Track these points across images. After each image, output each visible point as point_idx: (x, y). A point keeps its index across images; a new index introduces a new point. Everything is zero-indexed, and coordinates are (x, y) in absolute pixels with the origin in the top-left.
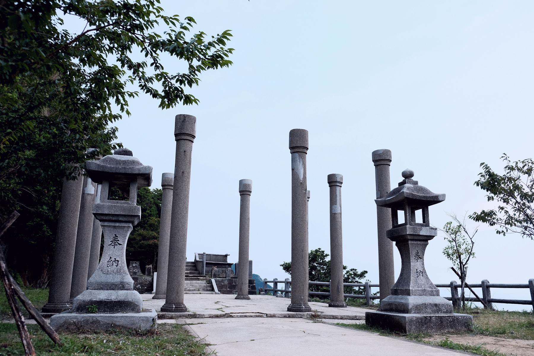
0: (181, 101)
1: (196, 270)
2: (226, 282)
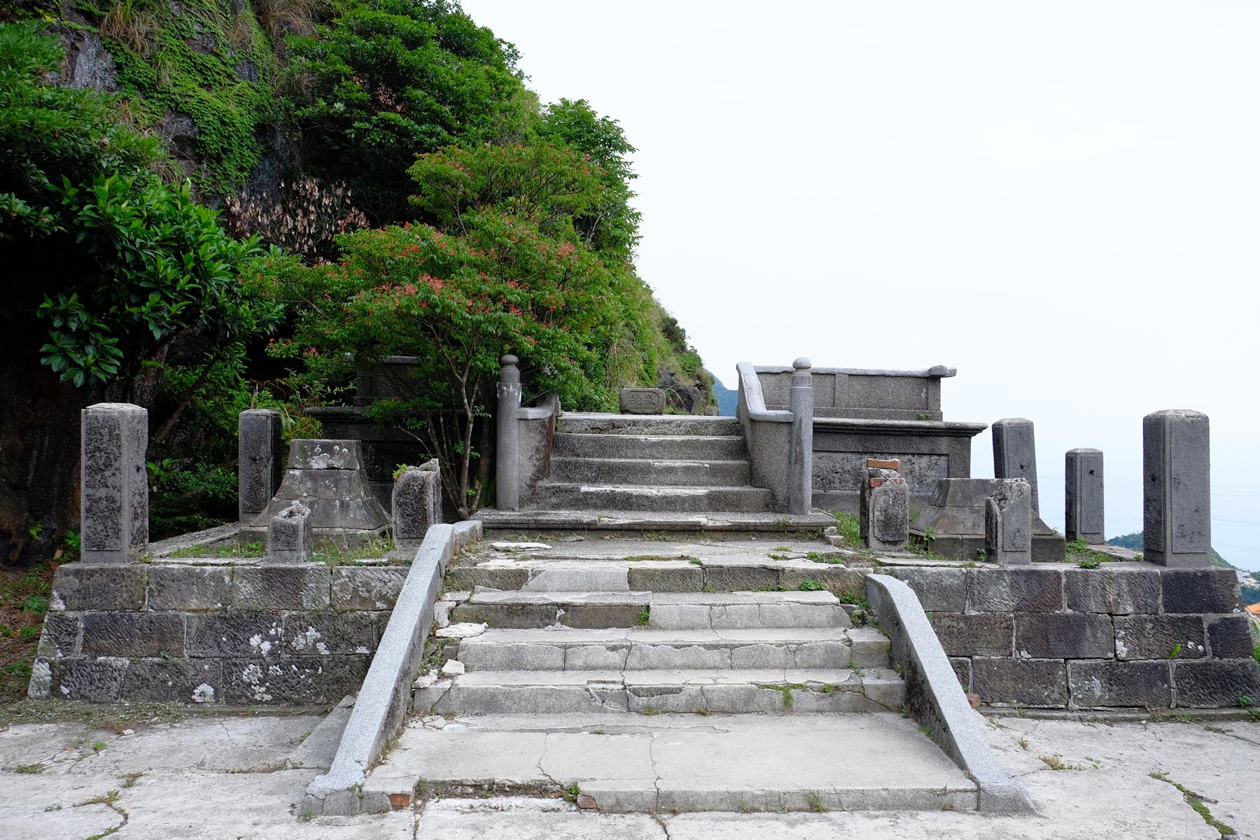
0: (390, 512)
1: (751, 476)
2: (1002, 600)
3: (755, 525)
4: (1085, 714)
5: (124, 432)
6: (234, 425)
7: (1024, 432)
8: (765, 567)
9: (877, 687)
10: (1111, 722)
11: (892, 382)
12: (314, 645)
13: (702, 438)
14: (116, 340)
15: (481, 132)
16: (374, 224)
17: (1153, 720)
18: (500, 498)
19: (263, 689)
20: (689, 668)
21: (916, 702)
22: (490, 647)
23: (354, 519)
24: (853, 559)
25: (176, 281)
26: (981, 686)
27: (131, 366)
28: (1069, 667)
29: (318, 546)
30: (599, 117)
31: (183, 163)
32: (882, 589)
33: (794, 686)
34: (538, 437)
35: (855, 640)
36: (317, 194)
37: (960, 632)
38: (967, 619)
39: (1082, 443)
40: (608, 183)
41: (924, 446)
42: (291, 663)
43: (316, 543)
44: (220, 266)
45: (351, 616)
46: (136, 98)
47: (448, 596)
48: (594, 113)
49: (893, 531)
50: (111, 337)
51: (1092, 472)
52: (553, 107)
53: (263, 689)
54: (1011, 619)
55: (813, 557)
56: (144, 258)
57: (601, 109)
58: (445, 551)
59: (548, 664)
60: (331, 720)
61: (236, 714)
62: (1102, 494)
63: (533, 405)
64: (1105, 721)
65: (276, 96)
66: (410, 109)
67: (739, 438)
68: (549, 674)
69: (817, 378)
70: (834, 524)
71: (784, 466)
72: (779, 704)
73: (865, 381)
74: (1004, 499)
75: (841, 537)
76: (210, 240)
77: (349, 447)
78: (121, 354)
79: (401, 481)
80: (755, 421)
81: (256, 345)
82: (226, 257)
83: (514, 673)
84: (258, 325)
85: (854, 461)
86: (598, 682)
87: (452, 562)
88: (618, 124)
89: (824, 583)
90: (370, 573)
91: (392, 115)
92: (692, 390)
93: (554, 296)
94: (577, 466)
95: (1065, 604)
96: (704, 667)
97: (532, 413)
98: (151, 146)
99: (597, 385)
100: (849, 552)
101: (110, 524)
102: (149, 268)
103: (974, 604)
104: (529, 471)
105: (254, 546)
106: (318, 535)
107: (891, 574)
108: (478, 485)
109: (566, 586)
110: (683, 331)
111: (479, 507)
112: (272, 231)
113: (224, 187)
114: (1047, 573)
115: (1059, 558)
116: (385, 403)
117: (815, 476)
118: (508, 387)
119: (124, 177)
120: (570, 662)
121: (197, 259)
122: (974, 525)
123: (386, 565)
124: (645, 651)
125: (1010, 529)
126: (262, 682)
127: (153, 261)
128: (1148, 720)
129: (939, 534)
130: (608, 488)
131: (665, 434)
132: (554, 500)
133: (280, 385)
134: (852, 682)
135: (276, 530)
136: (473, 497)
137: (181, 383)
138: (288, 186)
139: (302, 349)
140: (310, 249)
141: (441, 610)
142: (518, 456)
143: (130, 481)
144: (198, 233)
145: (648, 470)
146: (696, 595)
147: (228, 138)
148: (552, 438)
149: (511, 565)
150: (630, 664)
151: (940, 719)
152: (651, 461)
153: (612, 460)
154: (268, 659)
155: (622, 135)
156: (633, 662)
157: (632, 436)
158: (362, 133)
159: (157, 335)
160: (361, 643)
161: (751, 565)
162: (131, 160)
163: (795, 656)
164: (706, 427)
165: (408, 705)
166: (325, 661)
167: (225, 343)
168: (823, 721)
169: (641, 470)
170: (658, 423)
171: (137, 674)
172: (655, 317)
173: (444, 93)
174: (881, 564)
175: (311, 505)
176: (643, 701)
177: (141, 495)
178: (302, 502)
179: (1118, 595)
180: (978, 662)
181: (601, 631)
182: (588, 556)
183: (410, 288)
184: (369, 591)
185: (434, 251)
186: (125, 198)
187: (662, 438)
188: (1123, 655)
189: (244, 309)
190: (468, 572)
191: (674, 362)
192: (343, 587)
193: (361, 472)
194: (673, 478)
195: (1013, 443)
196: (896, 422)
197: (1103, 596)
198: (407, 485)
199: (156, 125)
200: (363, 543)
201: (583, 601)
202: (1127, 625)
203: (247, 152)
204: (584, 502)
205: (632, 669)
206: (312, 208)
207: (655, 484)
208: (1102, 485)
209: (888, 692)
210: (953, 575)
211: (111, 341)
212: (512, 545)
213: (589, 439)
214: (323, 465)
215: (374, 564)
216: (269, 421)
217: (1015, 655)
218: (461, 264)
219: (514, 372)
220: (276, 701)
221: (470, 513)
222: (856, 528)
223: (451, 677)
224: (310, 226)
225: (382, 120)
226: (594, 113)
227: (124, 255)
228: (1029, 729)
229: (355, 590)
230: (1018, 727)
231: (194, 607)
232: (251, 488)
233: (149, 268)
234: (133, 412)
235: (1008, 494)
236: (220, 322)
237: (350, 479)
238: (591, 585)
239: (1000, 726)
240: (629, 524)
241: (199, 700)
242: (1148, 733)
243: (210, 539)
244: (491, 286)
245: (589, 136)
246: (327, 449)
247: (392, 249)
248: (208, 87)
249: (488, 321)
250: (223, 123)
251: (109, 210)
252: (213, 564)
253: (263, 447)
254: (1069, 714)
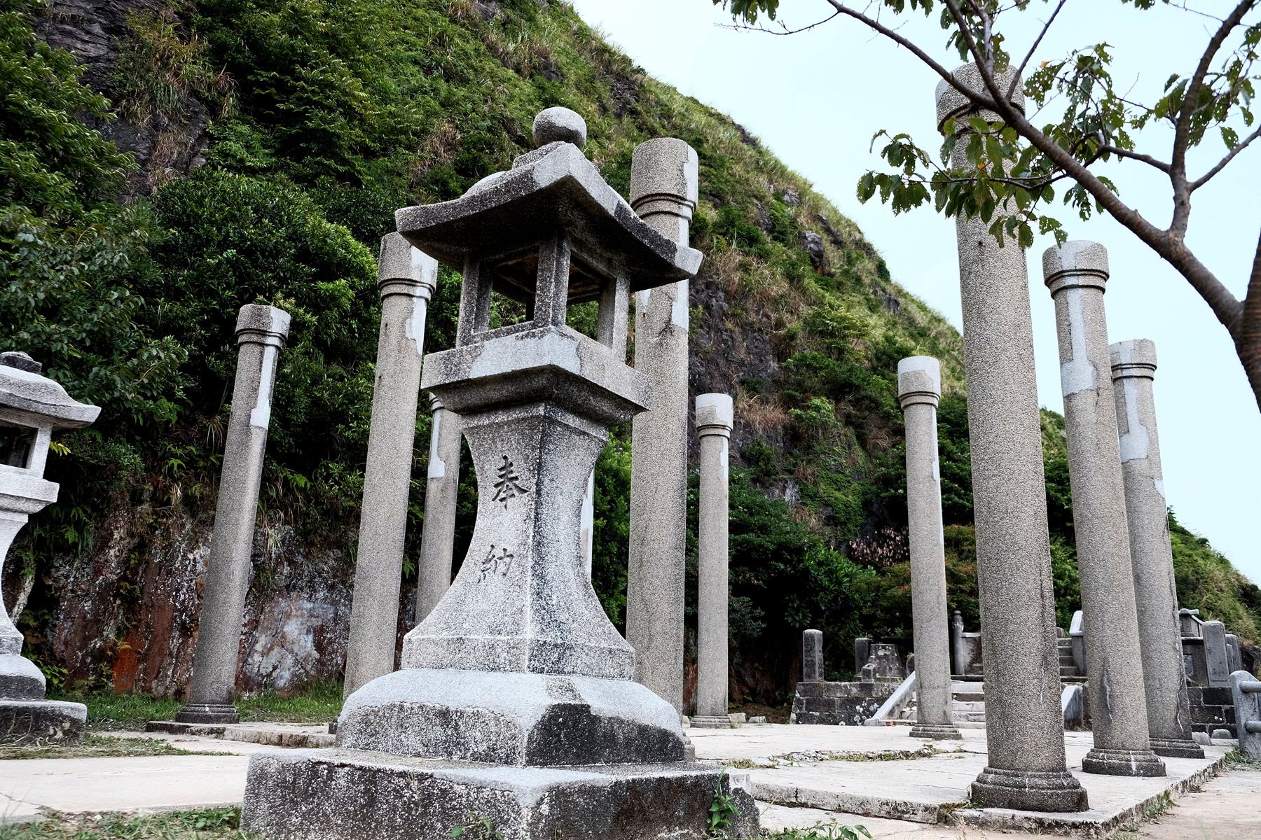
46: (809, 502)
97: (968, 635)
104: (968, 659)
248: (838, 490)
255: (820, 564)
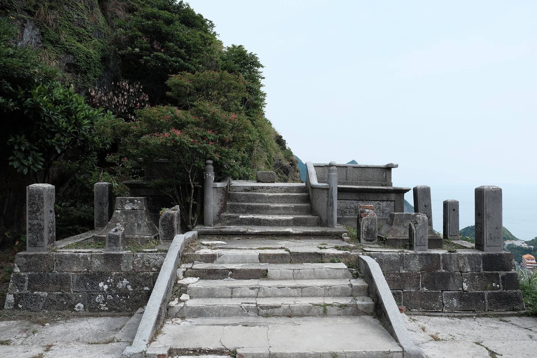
0: (158, 226)
1: (311, 211)
2: (415, 266)
3: (313, 232)
4: (450, 314)
5: (45, 196)
6: (92, 186)
7: (426, 192)
8: (316, 253)
9: (362, 305)
10: (460, 317)
11: (371, 170)
12: (126, 286)
13: (291, 194)
14: (41, 154)
15: (197, 61)
16: (153, 103)
17: (478, 316)
18: (205, 221)
19: (105, 305)
20: (284, 296)
21: (378, 312)
22: (201, 288)
23: (143, 231)
24: (354, 248)
25: (67, 128)
26: (407, 302)
27: (48, 165)
28: (443, 294)
29: (128, 243)
30: (248, 52)
31: (70, 74)
32: (365, 262)
33: (328, 305)
34: (222, 195)
35: (354, 284)
36: (127, 87)
37: (398, 280)
38: (401, 274)
39: (450, 198)
40: (252, 81)
41: (385, 198)
42: (116, 294)
43: (127, 241)
44: (86, 121)
45: (142, 274)
46: (50, 47)
47: (183, 266)
48: (246, 51)
49: (371, 236)
50: (39, 153)
51: (454, 210)
52: (229, 48)
53: (105, 305)
54: (419, 274)
55: (337, 248)
56: (53, 119)
57: (249, 49)
58: (181, 246)
59: (225, 295)
60: (133, 319)
61: (93, 316)
62: (458, 219)
63: (219, 181)
64: (458, 317)
65: (110, 45)
66: (167, 50)
67: (306, 194)
68: (225, 300)
69: (339, 169)
70: (346, 232)
71: (325, 207)
72: (321, 312)
73: (360, 170)
74: (417, 223)
75: (349, 238)
76: (81, 110)
77: (141, 200)
78: (44, 160)
79: (163, 215)
80: (313, 188)
81: (102, 154)
82: (88, 117)
83: (211, 299)
84: (102, 145)
85: (354, 204)
86: (246, 303)
87: (184, 251)
88: (256, 56)
89: (341, 259)
90: (150, 256)
91: (160, 54)
92: (288, 167)
93: (228, 137)
94: (238, 206)
95: (442, 268)
96: (291, 296)
97: (219, 185)
98: (56, 72)
99: (247, 168)
100: (352, 245)
101: (39, 235)
102: (56, 123)
103: (404, 268)
104: (217, 209)
105: (101, 243)
106: (127, 238)
107: (370, 255)
108: (196, 215)
109: (233, 261)
110: (285, 141)
111: (196, 225)
112: (108, 103)
113: (88, 84)
114: (434, 255)
115: (440, 247)
116: (156, 181)
117: (338, 210)
118: (208, 174)
119: (44, 85)
120: (234, 294)
121: (76, 118)
122: (404, 233)
123: (156, 252)
124: (265, 290)
125: (419, 236)
126: (104, 302)
127: (57, 121)
128: (476, 316)
129: (390, 237)
130: (251, 216)
131: (275, 192)
132: (228, 221)
133: (112, 169)
134: (352, 303)
135: (110, 238)
136: (194, 220)
137: (70, 169)
138: (115, 84)
139: (121, 158)
140: (125, 111)
141: (180, 272)
142: (213, 203)
143: (48, 218)
144: (76, 108)
145: (268, 208)
146: (287, 264)
147: (89, 63)
148: (228, 194)
149: (209, 252)
150: (259, 295)
151: (388, 320)
152: (269, 204)
153: (253, 204)
154: (107, 292)
155: (258, 61)
156: (261, 294)
157: (261, 193)
158: (147, 61)
159: (59, 152)
160: (146, 286)
161: (310, 252)
162: (48, 78)
163: (328, 291)
164: (293, 189)
165: (166, 313)
166: (131, 293)
167: (89, 153)
168: (340, 320)
169: (265, 208)
170: (272, 188)
171: (50, 299)
172: (273, 136)
173: (182, 45)
174: (365, 251)
175: (125, 226)
176: (265, 311)
177: (52, 223)
178: (121, 224)
179: (464, 264)
180: (405, 292)
181: (247, 281)
182: (242, 248)
183: (167, 134)
184: (149, 264)
185: (176, 118)
186: (45, 95)
187: (274, 194)
188: (466, 289)
189: (96, 139)
190: (191, 255)
191: (281, 155)
192: (138, 262)
193: (146, 211)
194: (279, 212)
195: (422, 195)
196: (373, 187)
197: (458, 264)
198: (166, 217)
199: (57, 58)
200: (147, 241)
201: (240, 268)
202: (467, 276)
203: (97, 69)
204: (241, 222)
205: (260, 297)
206: (125, 93)
207: (271, 214)
208: (458, 215)
209: (367, 307)
210: (395, 256)
211: (39, 154)
212: (210, 242)
213: (243, 195)
214: (130, 208)
215: (152, 252)
216: (107, 187)
217: (421, 289)
218: (188, 123)
219: (211, 167)
220: (110, 310)
221: (193, 227)
222: (355, 233)
223: (184, 301)
224: (125, 100)
225: (156, 56)
226: (246, 51)
227: (44, 118)
228: (426, 321)
229: (144, 263)
230: (421, 320)
231: (75, 270)
232: (100, 216)
233: (56, 123)
234: (49, 187)
235: (418, 221)
236: (86, 144)
237: (141, 214)
238: (243, 260)
239: (414, 320)
240: (260, 232)
241: (77, 310)
242: (476, 322)
243: (82, 239)
244: (201, 132)
245: (243, 63)
246: (132, 201)
247: (159, 116)
248: (81, 42)
249: (200, 148)
250: (87, 57)
251: (38, 100)
252: (83, 251)
253: (104, 198)
254: (443, 314)
255: (56, 103)
